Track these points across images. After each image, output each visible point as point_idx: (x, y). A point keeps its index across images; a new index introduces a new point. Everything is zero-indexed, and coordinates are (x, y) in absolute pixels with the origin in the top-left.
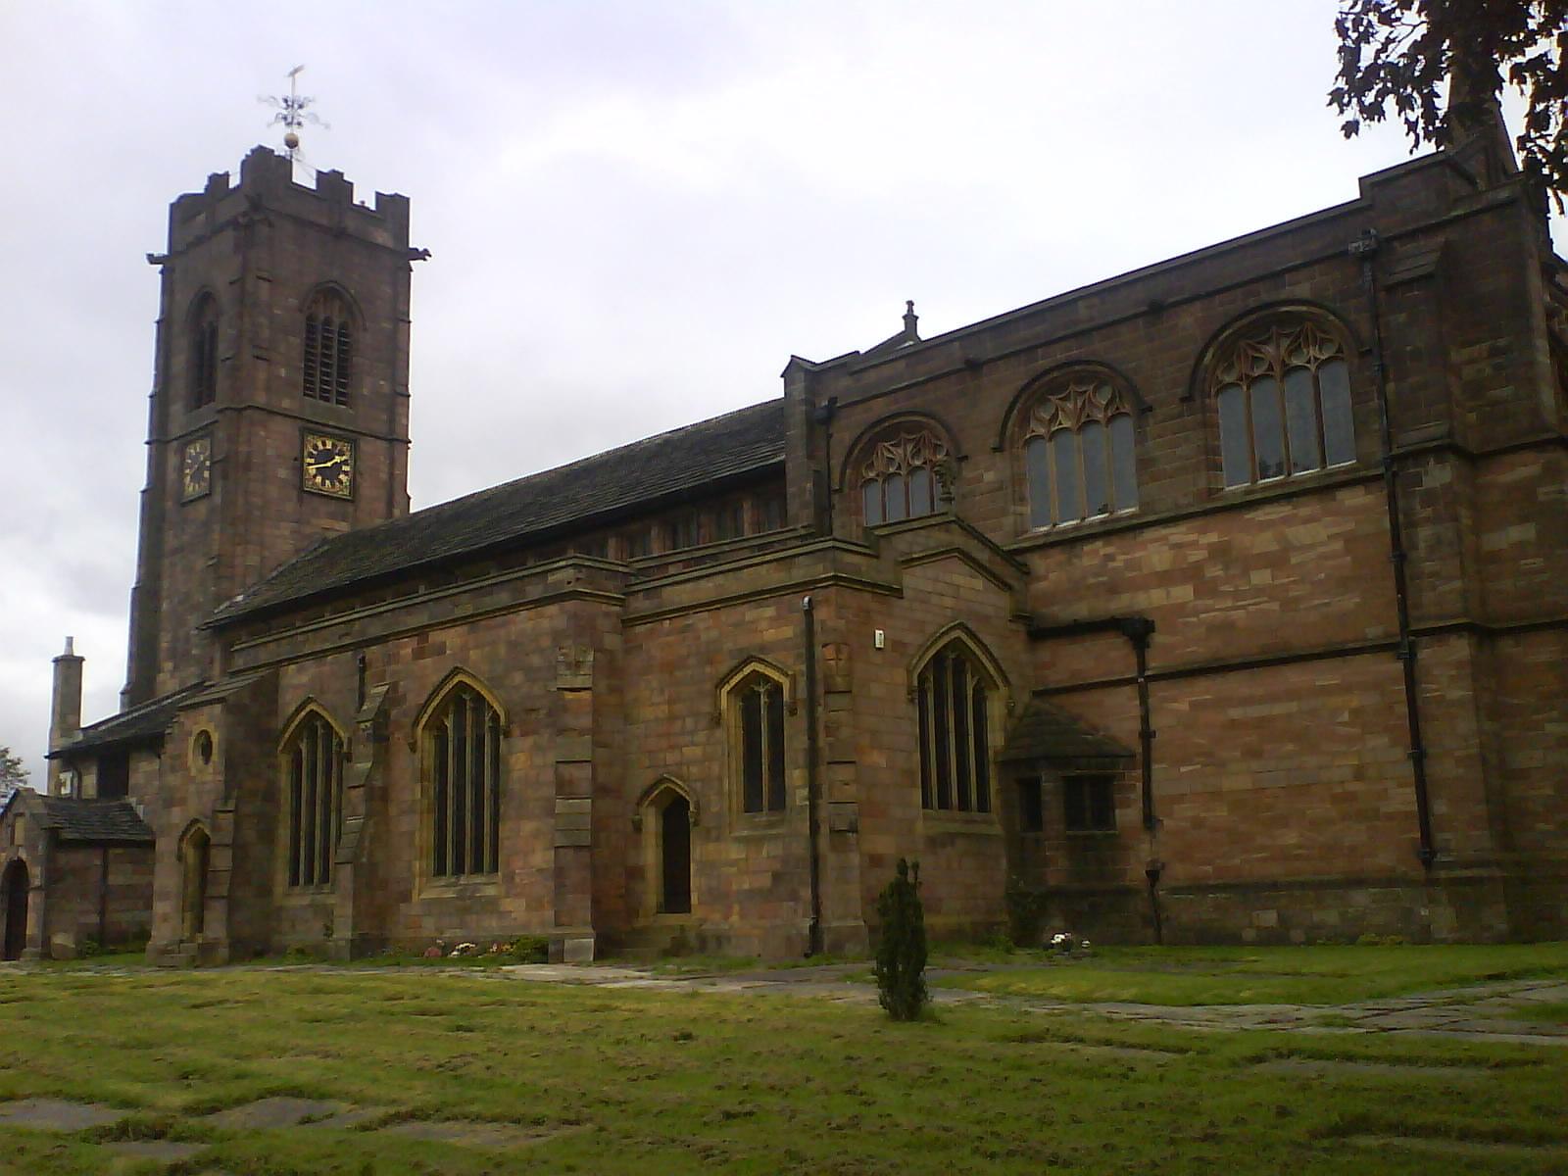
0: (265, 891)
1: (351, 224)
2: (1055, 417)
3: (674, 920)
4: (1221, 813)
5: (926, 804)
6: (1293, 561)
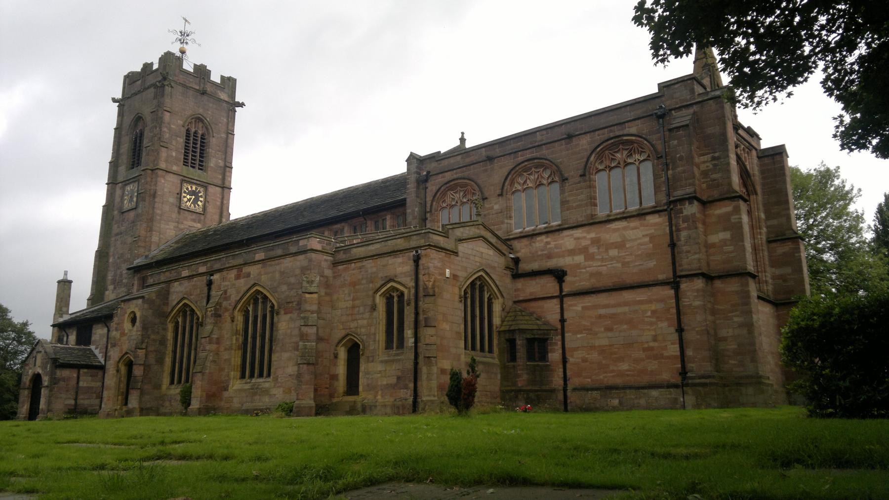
0: (158, 387)
1: (209, 89)
2: (525, 182)
3: (351, 398)
4: (594, 356)
5: (465, 348)
6: (627, 246)
